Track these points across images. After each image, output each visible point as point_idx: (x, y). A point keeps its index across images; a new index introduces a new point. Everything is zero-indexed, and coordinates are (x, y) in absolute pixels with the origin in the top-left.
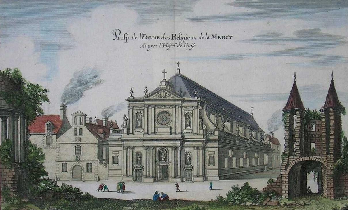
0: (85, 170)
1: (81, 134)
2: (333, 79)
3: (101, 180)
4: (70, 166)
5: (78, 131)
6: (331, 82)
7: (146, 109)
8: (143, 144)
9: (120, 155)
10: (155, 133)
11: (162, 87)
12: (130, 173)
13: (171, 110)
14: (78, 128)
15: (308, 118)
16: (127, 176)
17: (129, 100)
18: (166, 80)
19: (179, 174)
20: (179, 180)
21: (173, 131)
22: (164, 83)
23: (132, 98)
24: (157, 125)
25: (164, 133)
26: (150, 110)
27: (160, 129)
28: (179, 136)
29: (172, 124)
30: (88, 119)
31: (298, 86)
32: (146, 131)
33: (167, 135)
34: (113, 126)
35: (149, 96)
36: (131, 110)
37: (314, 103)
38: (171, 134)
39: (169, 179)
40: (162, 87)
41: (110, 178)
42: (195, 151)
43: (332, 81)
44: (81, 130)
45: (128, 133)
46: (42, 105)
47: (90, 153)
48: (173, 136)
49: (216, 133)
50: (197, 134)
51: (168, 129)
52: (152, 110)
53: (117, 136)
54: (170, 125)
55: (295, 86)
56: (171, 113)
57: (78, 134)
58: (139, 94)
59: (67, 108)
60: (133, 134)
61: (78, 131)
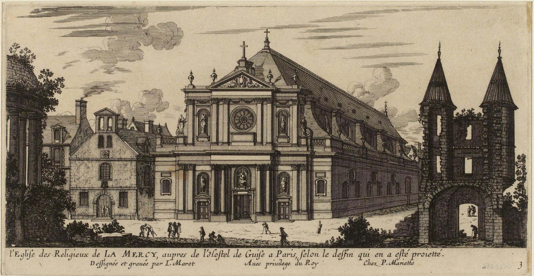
0: (117, 203)
1: (110, 145)
2: (501, 56)
3: (78, 237)
4: (92, 197)
5: (106, 140)
6: (497, 60)
7: (214, 106)
8: (210, 160)
9: (173, 178)
10: (229, 143)
11: (240, 69)
12: (190, 206)
13: (256, 108)
14: (105, 136)
15: (458, 123)
16: (184, 211)
17: (186, 91)
18: (246, 59)
19: (268, 210)
20: (268, 218)
21: (259, 139)
22: (243, 64)
23: (191, 87)
24: (232, 130)
25: (243, 142)
26: (221, 107)
27: (236, 138)
28: (269, 148)
29: (257, 129)
30: (121, 122)
31: (444, 66)
32: (214, 140)
33: (250, 146)
34: (159, 131)
35: (219, 85)
36: (191, 107)
37: (468, 95)
38: (255, 145)
39: (253, 217)
40: (240, 69)
41: (157, 216)
42: (295, 173)
43: (500, 58)
44: (110, 138)
45: (185, 144)
46: (142, 93)
47: (125, 176)
48: (258, 148)
49: (328, 143)
50: (298, 144)
51: (250, 138)
52: (223, 108)
53: (168, 149)
54: (254, 130)
55: (500, 67)
56: (255, 111)
57: (105, 144)
58: (203, 81)
59: (88, 105)
60: (193, 144)
61: (106, 140)
